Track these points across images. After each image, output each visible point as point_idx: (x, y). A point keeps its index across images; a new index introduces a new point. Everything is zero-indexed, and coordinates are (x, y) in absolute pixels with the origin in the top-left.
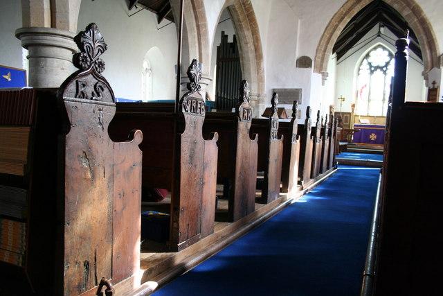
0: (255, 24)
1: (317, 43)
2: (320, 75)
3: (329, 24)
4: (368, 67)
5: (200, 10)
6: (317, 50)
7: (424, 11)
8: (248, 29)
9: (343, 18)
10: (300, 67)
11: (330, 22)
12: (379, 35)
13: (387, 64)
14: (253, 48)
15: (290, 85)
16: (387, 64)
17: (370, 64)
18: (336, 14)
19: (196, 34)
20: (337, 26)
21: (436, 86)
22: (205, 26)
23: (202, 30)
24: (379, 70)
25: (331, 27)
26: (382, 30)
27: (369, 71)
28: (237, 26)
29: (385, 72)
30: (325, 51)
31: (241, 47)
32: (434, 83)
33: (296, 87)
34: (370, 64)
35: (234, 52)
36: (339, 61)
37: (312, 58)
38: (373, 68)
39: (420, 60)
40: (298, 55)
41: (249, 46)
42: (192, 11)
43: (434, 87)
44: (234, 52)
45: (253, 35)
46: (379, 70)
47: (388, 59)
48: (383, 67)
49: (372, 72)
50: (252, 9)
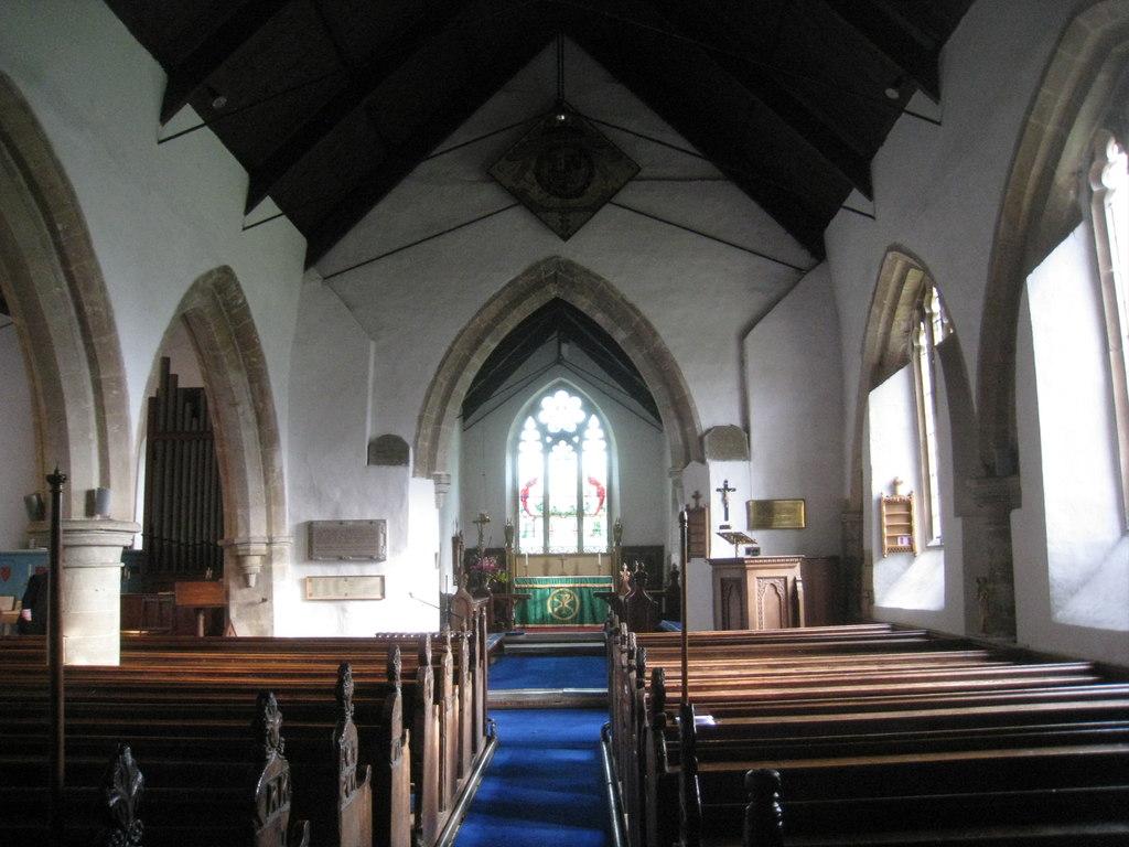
0: (260, 356)
1: (419, 403)
2: (430, 483)
3: (447, 356)
4: (537, 435)
5: (104, 340)
6: (421, 419)
7: (662, 333)
8: (238, 368)
9: (479, 342)
10: (378, 464)
11: (450, 350)
12: (559, 360)
13: (581, 428)
14: (251, 416)
15: (353, 513)
16: (581, 428)
17: (543, 429)
18: (462, 332)
19: (91, 405)
20: (468, 359)
21: (701, 504)
22: (120, 383)
23: (110, 396)
24: (563, 443)
25: (453, 364)
26: (565, 348)
27: (540, 446)
28: (209, 360)
29: (577, 448)
30: (439, 421)
31: (217, 413)
32: (697, 496)
33: (370, 516)
34: (543, 429)
35: (195, 413)
36: (470, 421)
37: (409, 439)
38: (553, 439)
39: (652, 418)
40: (371, 431)
41: (240, 410)
42: (80, 343)
43: (697, 506)
44: (195, 413)
45: (251, 381)
46: (563, 443)
47: (581, 416)
48: (573, 435)
49: (547, 448)
50: (249, 316)
